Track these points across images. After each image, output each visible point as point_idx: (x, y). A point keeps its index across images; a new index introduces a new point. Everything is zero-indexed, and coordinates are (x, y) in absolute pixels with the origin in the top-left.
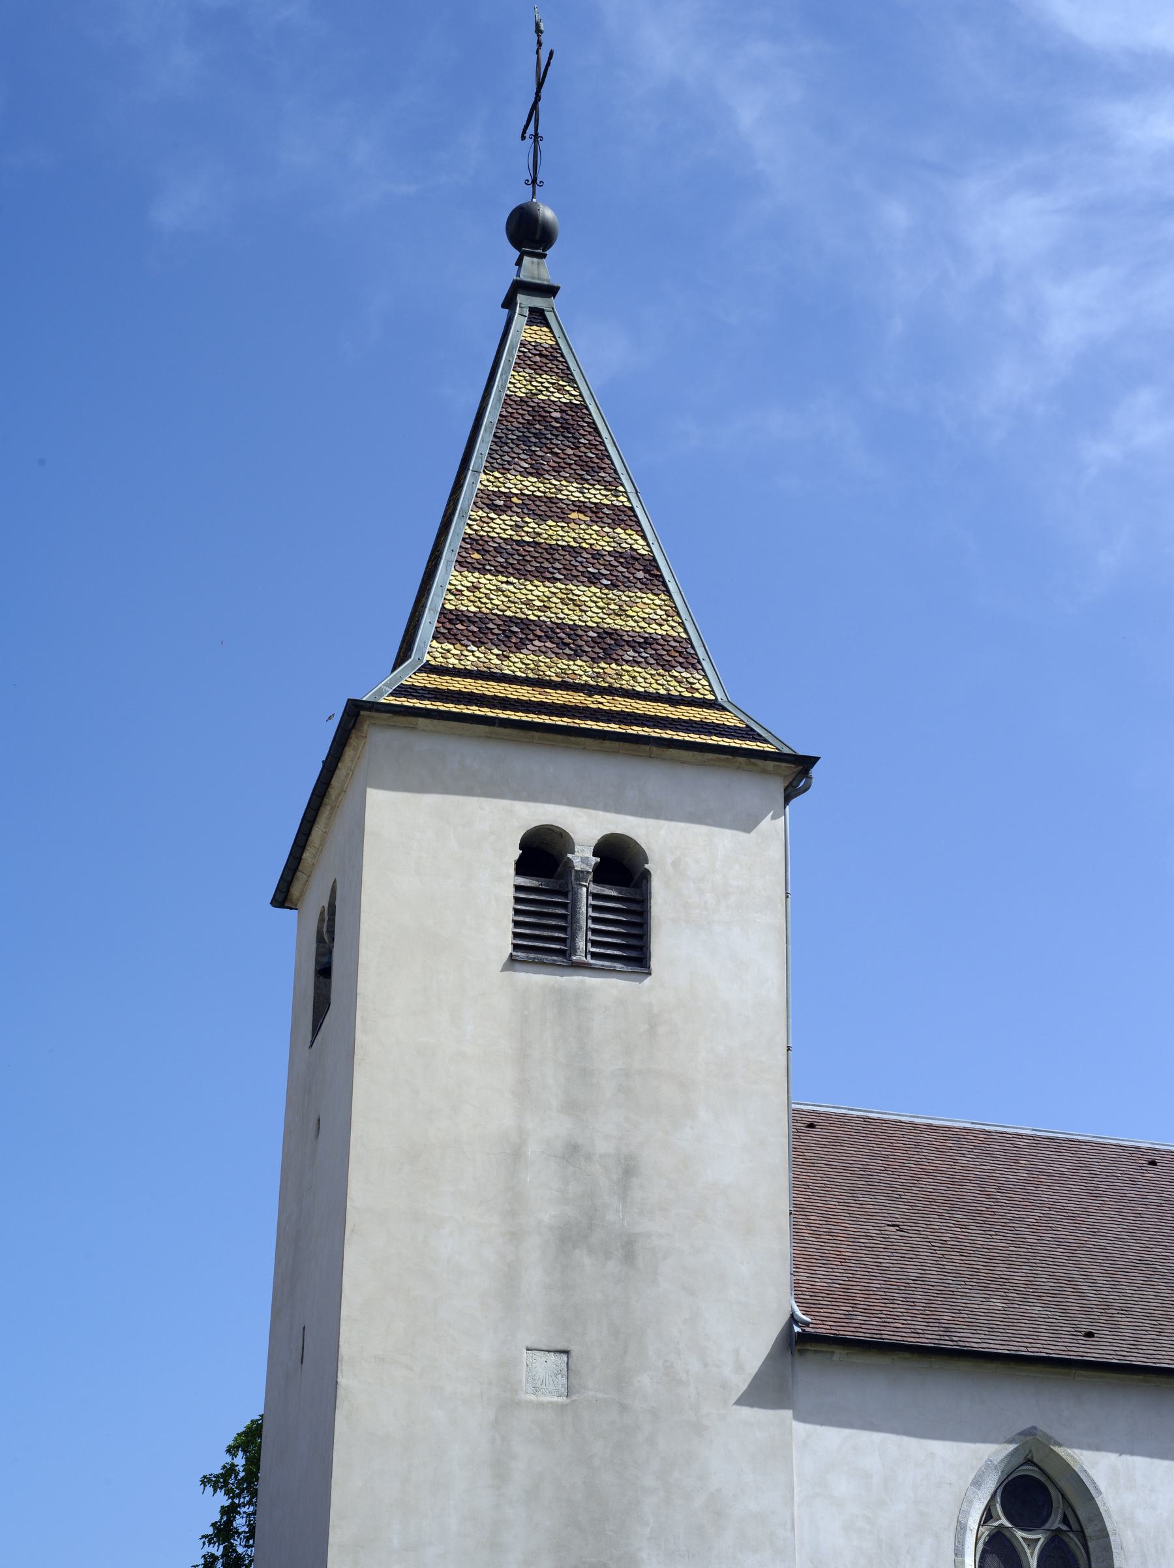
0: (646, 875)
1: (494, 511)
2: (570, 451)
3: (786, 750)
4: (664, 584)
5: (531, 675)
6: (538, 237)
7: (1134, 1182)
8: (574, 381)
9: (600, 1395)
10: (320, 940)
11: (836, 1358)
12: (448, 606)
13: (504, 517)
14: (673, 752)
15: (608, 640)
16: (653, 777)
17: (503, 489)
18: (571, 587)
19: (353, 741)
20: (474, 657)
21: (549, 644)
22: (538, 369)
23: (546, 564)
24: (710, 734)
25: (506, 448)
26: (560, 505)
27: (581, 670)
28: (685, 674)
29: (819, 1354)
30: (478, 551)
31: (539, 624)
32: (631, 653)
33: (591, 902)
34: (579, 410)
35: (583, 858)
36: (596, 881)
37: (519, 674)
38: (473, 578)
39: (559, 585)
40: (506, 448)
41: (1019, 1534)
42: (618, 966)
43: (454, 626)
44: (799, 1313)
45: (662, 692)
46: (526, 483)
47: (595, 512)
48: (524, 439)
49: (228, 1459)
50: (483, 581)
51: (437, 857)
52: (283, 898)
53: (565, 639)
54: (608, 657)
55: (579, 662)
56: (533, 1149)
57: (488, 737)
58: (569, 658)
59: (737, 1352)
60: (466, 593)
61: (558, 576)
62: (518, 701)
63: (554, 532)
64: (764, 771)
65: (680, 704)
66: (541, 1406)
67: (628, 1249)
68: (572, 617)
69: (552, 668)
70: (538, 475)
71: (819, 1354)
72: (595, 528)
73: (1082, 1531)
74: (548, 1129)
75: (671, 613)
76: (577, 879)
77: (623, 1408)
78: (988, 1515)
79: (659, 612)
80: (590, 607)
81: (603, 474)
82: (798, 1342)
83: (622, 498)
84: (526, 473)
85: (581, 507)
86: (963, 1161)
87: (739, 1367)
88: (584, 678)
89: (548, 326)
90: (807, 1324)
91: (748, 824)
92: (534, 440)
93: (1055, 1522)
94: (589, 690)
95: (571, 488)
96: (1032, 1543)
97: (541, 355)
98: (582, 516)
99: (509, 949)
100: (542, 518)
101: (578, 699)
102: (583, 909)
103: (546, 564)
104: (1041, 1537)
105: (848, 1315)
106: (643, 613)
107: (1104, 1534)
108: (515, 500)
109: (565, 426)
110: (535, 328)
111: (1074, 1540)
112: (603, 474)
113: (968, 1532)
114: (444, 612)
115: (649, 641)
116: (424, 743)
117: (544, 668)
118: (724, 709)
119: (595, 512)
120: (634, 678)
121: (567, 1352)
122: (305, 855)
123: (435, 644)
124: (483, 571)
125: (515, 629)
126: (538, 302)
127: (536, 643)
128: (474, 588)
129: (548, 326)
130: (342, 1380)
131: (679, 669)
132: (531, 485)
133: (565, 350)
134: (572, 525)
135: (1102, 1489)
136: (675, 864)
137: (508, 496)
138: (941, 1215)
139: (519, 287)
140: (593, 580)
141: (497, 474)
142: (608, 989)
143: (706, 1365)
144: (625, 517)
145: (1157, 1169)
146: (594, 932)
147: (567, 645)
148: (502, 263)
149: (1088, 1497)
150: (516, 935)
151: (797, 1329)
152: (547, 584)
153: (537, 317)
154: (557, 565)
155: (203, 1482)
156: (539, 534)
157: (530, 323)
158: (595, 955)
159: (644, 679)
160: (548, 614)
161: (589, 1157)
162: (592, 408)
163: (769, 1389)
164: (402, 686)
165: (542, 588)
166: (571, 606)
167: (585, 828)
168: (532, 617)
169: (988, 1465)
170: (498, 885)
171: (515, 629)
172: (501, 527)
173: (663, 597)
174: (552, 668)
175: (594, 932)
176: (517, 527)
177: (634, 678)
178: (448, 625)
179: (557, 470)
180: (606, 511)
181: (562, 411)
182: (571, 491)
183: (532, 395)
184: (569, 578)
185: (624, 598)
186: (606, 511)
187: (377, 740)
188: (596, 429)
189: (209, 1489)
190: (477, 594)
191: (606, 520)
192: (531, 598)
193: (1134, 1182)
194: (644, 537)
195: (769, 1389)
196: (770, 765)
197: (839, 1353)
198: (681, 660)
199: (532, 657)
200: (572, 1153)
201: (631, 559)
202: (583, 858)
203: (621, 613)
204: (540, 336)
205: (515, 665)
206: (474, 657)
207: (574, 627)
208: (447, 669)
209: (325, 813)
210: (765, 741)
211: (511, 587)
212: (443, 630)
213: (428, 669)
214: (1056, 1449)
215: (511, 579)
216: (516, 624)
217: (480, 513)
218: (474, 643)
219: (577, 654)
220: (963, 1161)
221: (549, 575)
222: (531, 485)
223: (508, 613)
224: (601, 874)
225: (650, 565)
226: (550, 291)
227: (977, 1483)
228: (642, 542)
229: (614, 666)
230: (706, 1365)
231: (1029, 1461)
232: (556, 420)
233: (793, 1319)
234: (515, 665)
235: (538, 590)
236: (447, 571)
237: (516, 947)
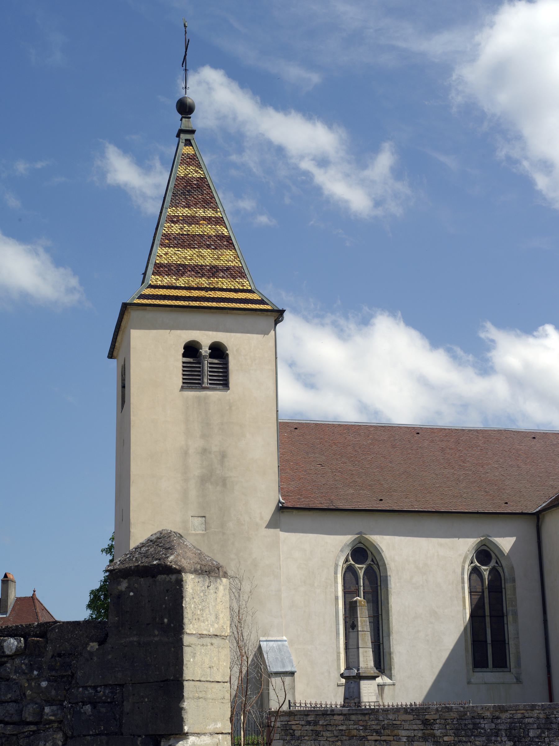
0: (227, 355)
1: (173, 223)
2: (200, 197)
3: (276, 309)
4: (234, 246)
5: (186, 285)
6: (187, 110)
7: (409, 441)
8: (201, 168)
9: (216, 530)
10: (122, 376)
11: (294, 513)
12: (157, 262)
13: (177, 225)
14: (235, 311)
15: (214, 270)
16: (229, 320)
17: (176, 214)
18: (201, 250)
19: (126, 313)
20: (167, 280)
21: (193, 273)
22: (189, 164)
23: (192, 242)
24: (248, 303)
25: (177, 198)
26: (197, 218)
27: (204, 282)
28: (241, 280)
29: (290, 512)
30: (167, 239)
31: (189, 265)
32: (222, 274)
33: (209, 365)
34: (202, 180)
35: (205, 351)
36: (210, 358)
37: (182, 285)
38: (166, 250)
39: (196, 250)
40: (177, 198)
41: (357, 565)
42: (218, 387)
43: (160, 269)
44: (281, 500)
45: (233, 288)
46: (184, 211)
47: (209, 220)
48: (183, 193)
49: (110, 542)
50: (169, 251)
51: (156, 351)
52: (111, 355)
53: (198, 270)
54: (214, 276)
55: (203, 279)
56: (191, 451)
57: (171, 311)
58: (200, 277)
59: (261, 513)
60: (164, 256)
61: (196, 246)
62: (181, 296)
63: (195, 229)
64: (267, 315)
65: (238, 292)
66: (197, 534)
67: (224, 482)
68: (201, 262)
69: (194, 282)
70: (189, 207)
71: (290, 512)
72: (209, 226)
73: (378, 564)
74: (196, 444)
75: (236, 257)
76: (204, 358)
77: (224, 534)
78: (347, 560)
79: (232, 257)
80: (207, 257)
81: (212, 205)
82: (281, 509)
83: (219, 214)
84: (184, 207)
85: (204, 218)
86: (349, 438)
87: (262, 518)
88: (205, 285)
89: (192, 146)
90: (284, 503)
92: (187, 193)
93: (369, 561)
94: (206, 289)
95: (200, 211)
96: (361, 568)
97: (189, 158)
98: (204, 222)
99: (181, 384)
100: (190, 224)
101: (203, 293)
102: (206, 368)
103: (192, 242)
104: (364, 566)
105: (299, 499)
106: (227, 258)
107: (384, 565)
108: (180, 218)
109: (198, 186)
110: (187, 147)
111: (375, 567)
112: (212, 205)
113: (339, 567)
114: (156, 264)
115: (228, 269)
116: (149, 315)
117: (191, 282)
118: (254, 293)
119: (209, 220)
120: (223, 283)
121: (204, 517)
122: (116, 344)
123: (153, 277)
124: (169, 247)
125: (181, 268)
126: (188, 136)
127: (188, 273)
128: (166, 254)
129: (192, 146)
130: (132, 530)
131: (239, 278)
132: (186, 212)
133: (198, 156)
134: (201, 226)
135: (384, 550)
136: (237, 350)
137: (178, 216)
138: (337, 459)
139: (181, 131)
140: (208, 247)
141: (174, 208)
142: (215, 395)
143: (250, 518)
144: (219, 221)
145: (419, 435)
146: (210, 376)
147: (199, 273)
148: (176, 120)
149: (380, 553)
150: (183, 379)
151: (280, 505)
152: (192, 250)
153: (188, 143)
154: (196, 242)
155: (102, 551)
156: (189, 231)
157: (186, 145)
158: (210, 384)
159: (226, 283)
160: (193, 261)
161: (210, 453)
162: (208, 178)
163: (273, 524)
164: (141, 295)
165: (190, 252)
166: (201, 258)
167: (205, 339)
168: (187, 263)
169: (475, 542)
170: (176, 361)
171: (181, 268)
172: (176, 229)
173: (233, 251)
174: (194, 282)
175: (210, 376)
176: (181, 229)
177: (223, 283)
178: (157, 269)
179: (196, 204)
180: (213, 219)
181: (197, 181)
182: (201, 213)
183: (186, 175)
184: (200, 247)
185: (219, 253)
186: (213, 219)
187: (133, 315)
188: (209, 187)
189: (104, 553)
190: (167, 256)
191: (213, 223)
192: (186, 256)
193: (409, 441)
194: (227, 228)
195: (273, 524)
196: (269, 313)
197: (295, 512)
198: (239, 275)
199: (187, 278)
200: (205, 451)
201: (221, 237)
202: (205, 351)
203: (218, 259)
204: (188, 150)
205: (181, 282)
206: (167, 280)
207: (202, 266)
208: (157, 286)
209: (120, 333)
210: (268, 304)
211: (179, 252)
212: (156, 271)
213: (151, 286)
214: (367, 536)
215: (180, 249)
216: (181, 266)
217: (168, 224)
218: (166, 275)
219: (203, 276)
220: (349, 438)
221: (192, 246)
222: (186, 212)
223: (178, 262)
224: (211, 356)
225: (229, 239)
226: (193, 132)
227: (342, 551)
228: (226, 230)
229: (216, 279)
230: (250, 518)
231: (360, 543)
232: (195, 184)
233: (279, 502)
234: (181, 282)
235: (188, 253)
236: (157, 249)
237: (183, 383)
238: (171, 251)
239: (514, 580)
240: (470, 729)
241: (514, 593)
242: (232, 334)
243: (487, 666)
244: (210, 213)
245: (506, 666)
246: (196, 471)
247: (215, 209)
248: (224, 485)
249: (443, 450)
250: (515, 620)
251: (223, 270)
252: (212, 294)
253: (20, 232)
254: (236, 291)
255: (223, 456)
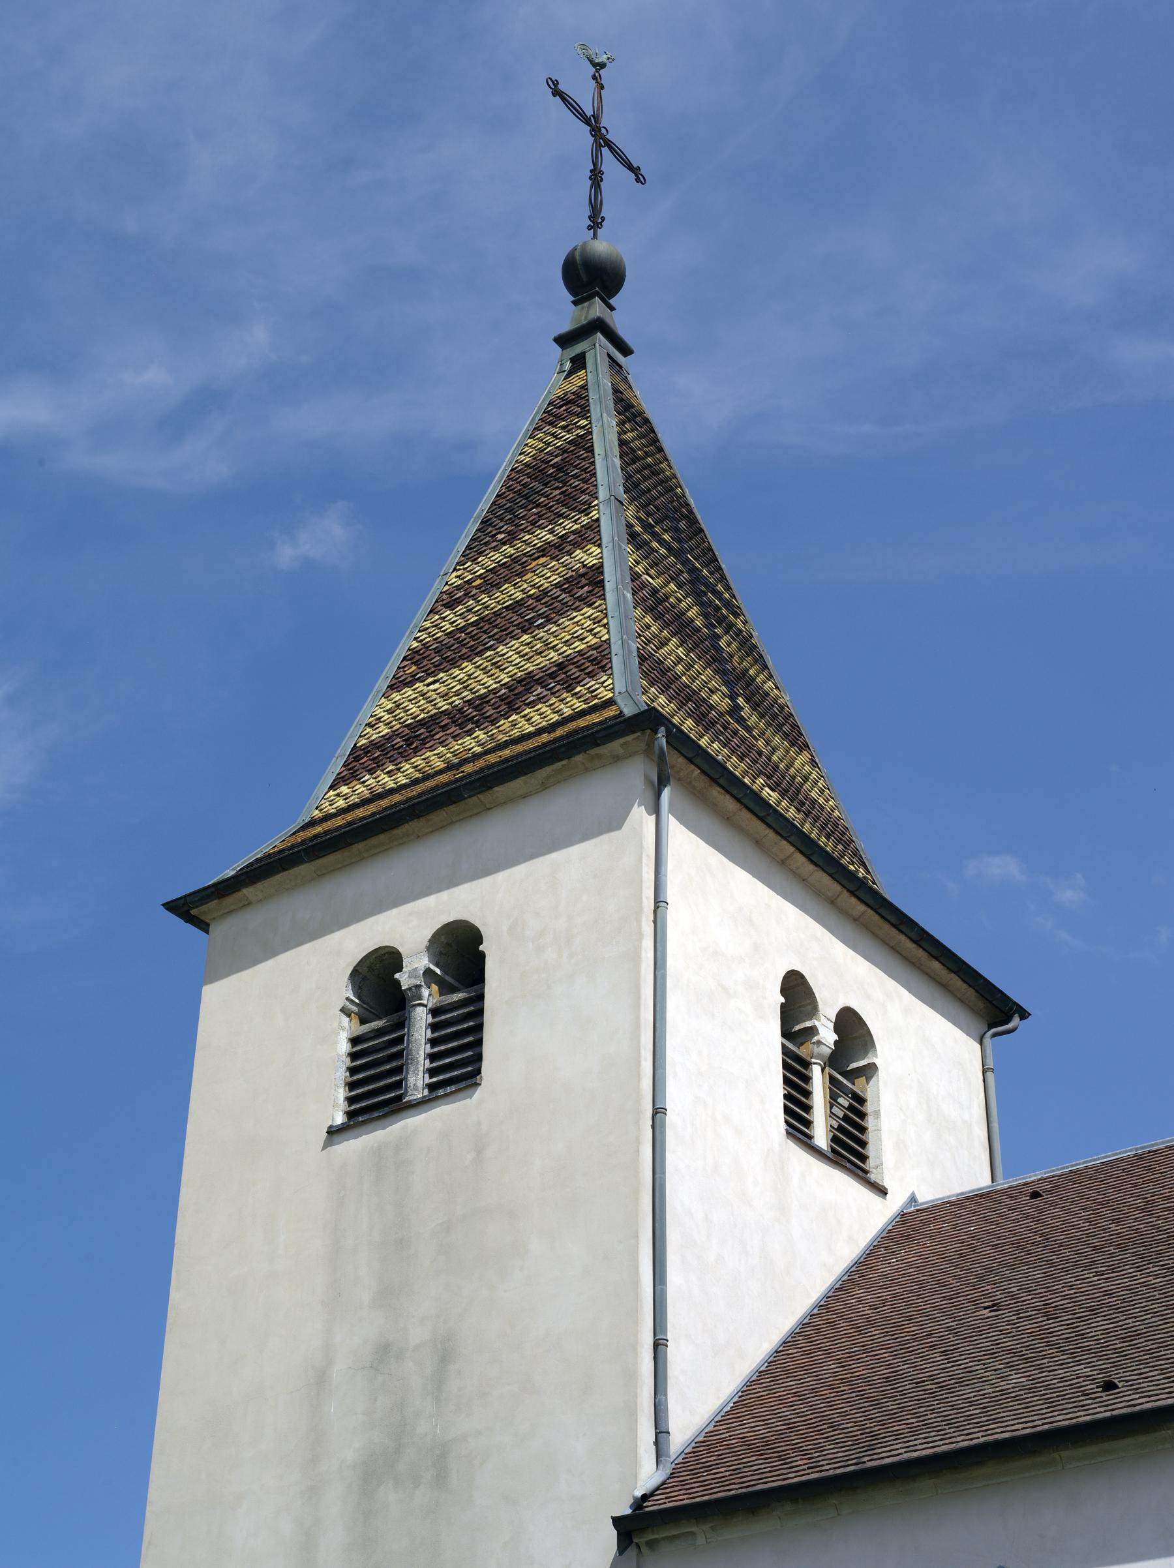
11: (700, 1540)
32: (540, 690)
51: (273, 1022)
91: (614, 822)
148: (565, 313)
200: (385, 1354)
202: (417, 963)
242: (501, 876)
246: (347, 1447)
248: (441, 1477)
251: (541, 682)
255: (445, 1353)
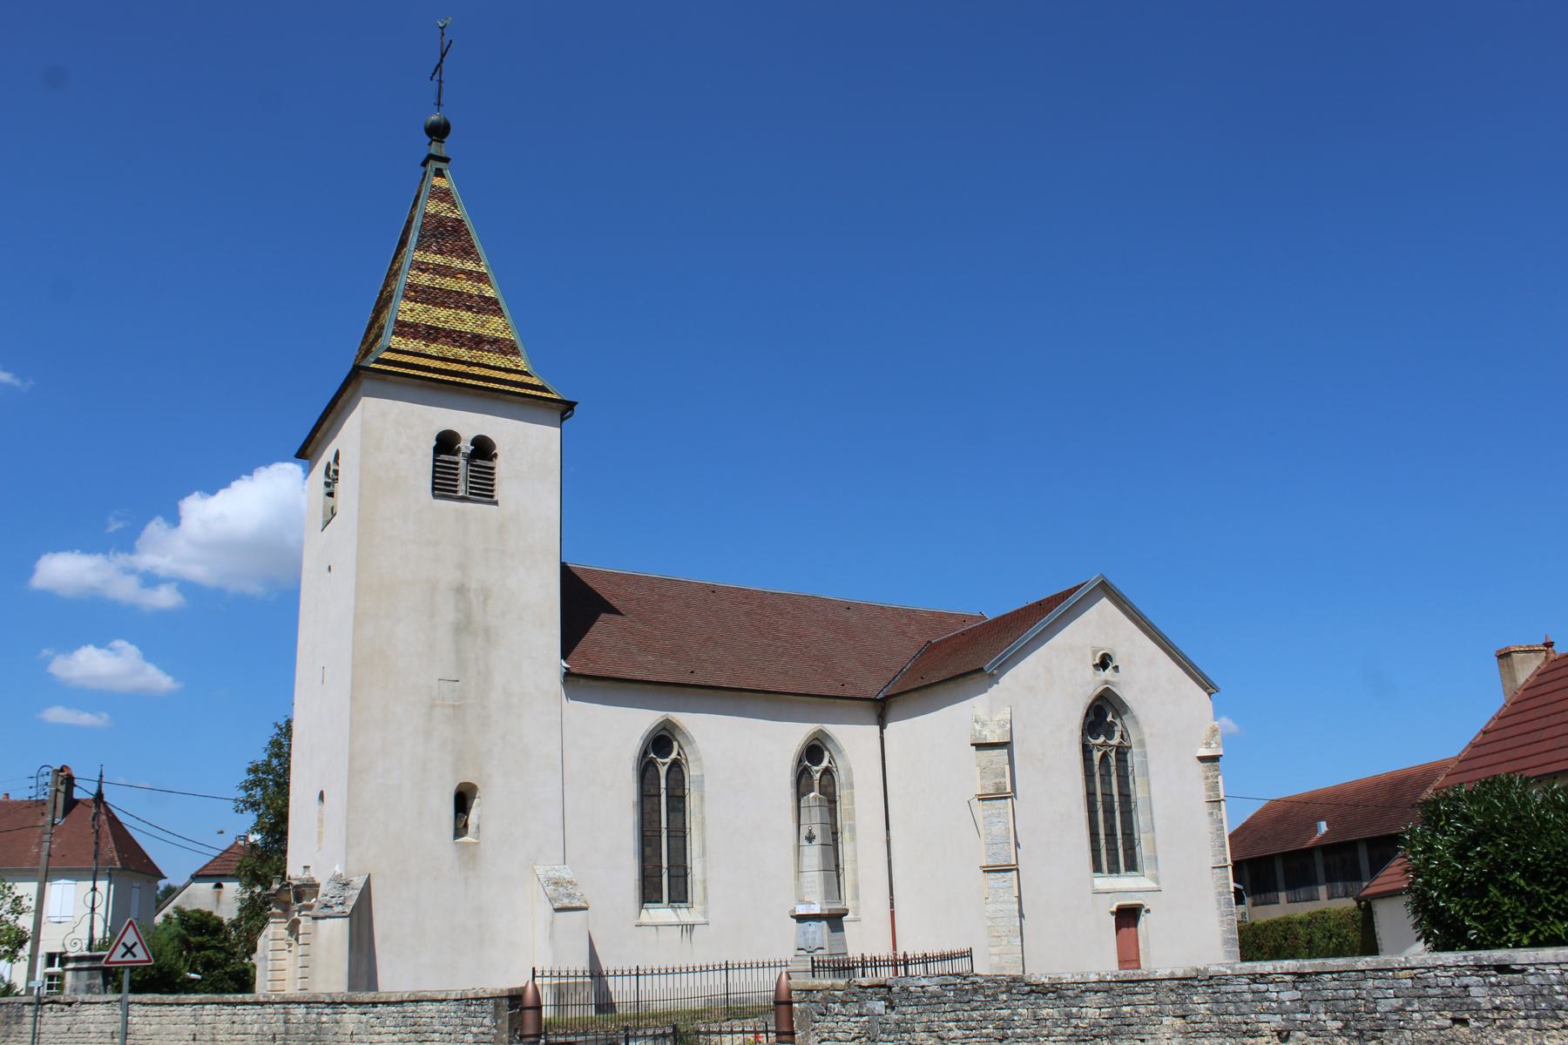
20: (412, 345)
22: (442, 200)
27: (463, 353)
35: (466, 446)
63: (449, 283)
69: (452, 352)
85: (463, 272)
101: (463, 368)
102: (463, 470)
115: (496, 341)
132: (439, 259)
139: (431, 157)
140: (469, 309)
172: (424, 279)
174: (452, 352)
182: (457, 263)
184: (457, 307)
197: (582, 681)
205: (433, 349)
206: (412, 345)
213: (390, 350)
222: (439, 259)
234: (433, 349)
235: (442, 313)
238: (419, 307)
239: (851, 786)
240: (1246, 1002)
241: (852, 803)
243: (660, 901)
244: (470, 266)
245: (685, 900)
247: (478, 261)
249: (748, 613)
250: (853, 839)
251: (489, 342)
252: (477, 371)
253: (5, 370)
254: (470, 364)
255: (486, 595)
